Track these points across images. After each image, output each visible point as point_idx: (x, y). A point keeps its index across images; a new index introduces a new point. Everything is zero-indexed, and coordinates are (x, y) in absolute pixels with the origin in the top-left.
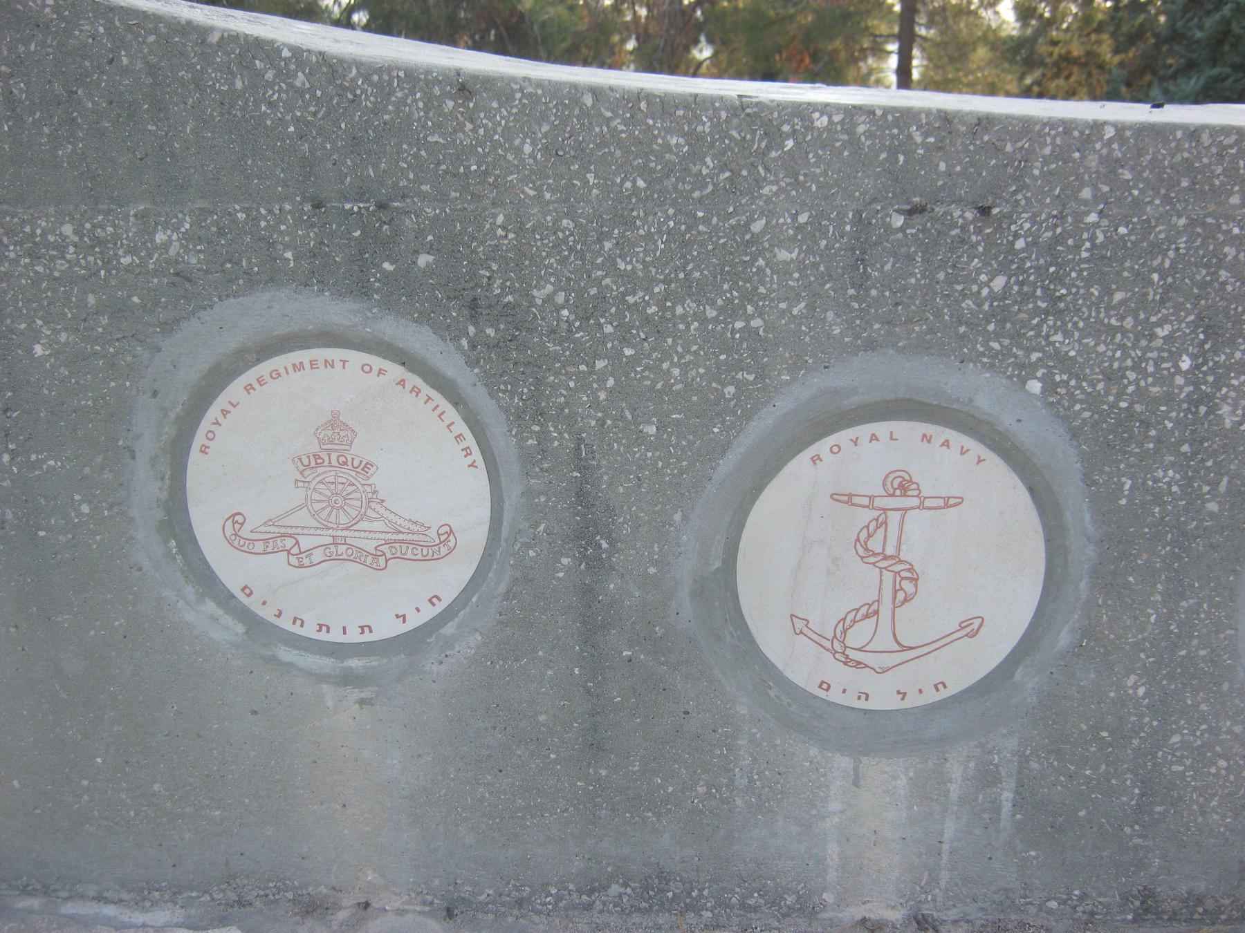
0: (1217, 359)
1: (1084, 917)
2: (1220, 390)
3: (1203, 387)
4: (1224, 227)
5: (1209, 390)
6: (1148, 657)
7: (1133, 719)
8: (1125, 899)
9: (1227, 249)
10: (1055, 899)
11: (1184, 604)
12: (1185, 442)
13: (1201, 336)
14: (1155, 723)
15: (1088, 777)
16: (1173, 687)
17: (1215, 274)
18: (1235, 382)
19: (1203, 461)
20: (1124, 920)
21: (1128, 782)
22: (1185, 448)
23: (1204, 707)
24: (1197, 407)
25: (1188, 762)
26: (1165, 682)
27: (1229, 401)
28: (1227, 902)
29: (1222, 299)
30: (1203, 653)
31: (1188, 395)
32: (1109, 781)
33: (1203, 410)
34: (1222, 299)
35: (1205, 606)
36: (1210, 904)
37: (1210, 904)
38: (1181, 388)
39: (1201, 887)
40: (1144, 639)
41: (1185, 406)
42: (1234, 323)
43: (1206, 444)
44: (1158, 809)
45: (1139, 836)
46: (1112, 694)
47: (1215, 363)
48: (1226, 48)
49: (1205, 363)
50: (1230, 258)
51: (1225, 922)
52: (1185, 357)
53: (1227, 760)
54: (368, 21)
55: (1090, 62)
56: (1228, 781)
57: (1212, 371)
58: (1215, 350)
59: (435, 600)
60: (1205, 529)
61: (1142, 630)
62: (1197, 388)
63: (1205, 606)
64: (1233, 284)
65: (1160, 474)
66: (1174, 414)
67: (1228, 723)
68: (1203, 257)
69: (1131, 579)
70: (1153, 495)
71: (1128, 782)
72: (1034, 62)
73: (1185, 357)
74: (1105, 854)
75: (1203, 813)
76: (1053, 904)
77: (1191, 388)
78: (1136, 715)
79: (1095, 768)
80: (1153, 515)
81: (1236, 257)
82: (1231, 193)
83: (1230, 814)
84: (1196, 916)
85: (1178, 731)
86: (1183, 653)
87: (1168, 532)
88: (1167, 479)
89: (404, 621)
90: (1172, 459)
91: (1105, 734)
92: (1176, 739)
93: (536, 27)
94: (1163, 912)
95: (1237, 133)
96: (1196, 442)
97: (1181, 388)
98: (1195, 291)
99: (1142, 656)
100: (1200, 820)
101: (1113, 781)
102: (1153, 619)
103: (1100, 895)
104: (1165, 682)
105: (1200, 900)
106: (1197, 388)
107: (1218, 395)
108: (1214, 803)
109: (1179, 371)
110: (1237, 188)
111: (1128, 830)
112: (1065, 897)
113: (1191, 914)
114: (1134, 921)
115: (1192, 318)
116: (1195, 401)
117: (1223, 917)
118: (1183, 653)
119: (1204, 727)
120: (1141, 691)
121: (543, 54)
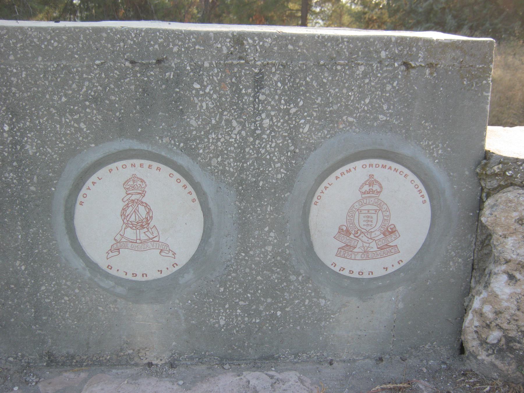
0: (19, 125)
1: (25, 365)
2: (24, 139)
3: (16, 138)
4: (9, 69)
5: (19, 139)
6: (22, 253)
7: (23, 279)
8: (41, 357)
9: (12, 79)
10: (11, 357)
11: (31, 230)
12: (14, 161)
13: (10, 116)
14: (33, 281)
15: (10, 305)
16: (36, 266)
17: (10, 89)
18: (29, 135)
19: (24, 169)
20: (43, 365)
21: (28, 307)
22: (15, 164)
23: (51, 274)
24: (16, 146)
25: (52, 298)
26: (32, 264)
27: (29, 143)
28: (85, 357)
29: (15, 100)
30: (45, 251)
31: (11, 141)
32: (20, 306)
33: (18, 147)
34: (15, 100)
35: (41, 231)
36: (77, 358)
37: (77, 358)
38: (7, 138)
39: (72, 351)
40: (18, 245)
41: (10, 146)
42: (23, 110)
43: (23, 162)
44: (44, 318)
45: (40, 330)
46: (11, 269)
47: (19, 127)
48: (432, 15)
49: (15, 127)
50: (14, 82)
51: (86, 366)
52: (5, 125)
53: (68, 297)
54: (307, 16)
55: (384, 23)
56: (71, 305)
57: (19, 130)
58: (18, 122)
59: (175, 265)
60: (32, 198)
61: (16, 242)
62: (14, 138)
63: (41, 231)
64: (19, 94)
65: (7, 175)
66: (6, 149)
67: (64, 281)
68: (3, 82)
69: (6, 220)
70: (6, 184)
71: (28, 307)
72: (363, 21)
73: (5, 125)
74: (27, 337)
75: (64, 320)
76: (11, 359)
77: (11, 138)
78: (24, 278)
79: (13, 301)
80: (8, 192)
81: (17, 82)
82: (9, 55)
83: (75, 320)
84: (73, 364)
85: (43, 284)
86: (36, 251)
87: (16, 200)
88: (11, 177)
89: (161, 273)
90: (11, 168)
91: (12, 286)
92: (43, 288)
93: (152, 7)
94: (59, 362)
95: (6, 29)
96: (20, 161)
97: (7, 138)
98: (3, 96)
99: (19, 252)
100: (63, 322)
101: (22, 306)
102: (20, 236)
103: (30, 355)
104: (32, 264)
105: (73, 357)
106: (14, 138)
107: (24, 141)
108: (67, 315)
109: (4, 131)
110: (11, 53)
111: (34, 327)
112: (15, 356)
113: (71, 363)
114: (48, 365)
115: (4, 108)
116: (15, 144)
117: (85, 364)
118: (36, 251)
119: (54, 283)
120: (23, 268)
121: (155, 17)
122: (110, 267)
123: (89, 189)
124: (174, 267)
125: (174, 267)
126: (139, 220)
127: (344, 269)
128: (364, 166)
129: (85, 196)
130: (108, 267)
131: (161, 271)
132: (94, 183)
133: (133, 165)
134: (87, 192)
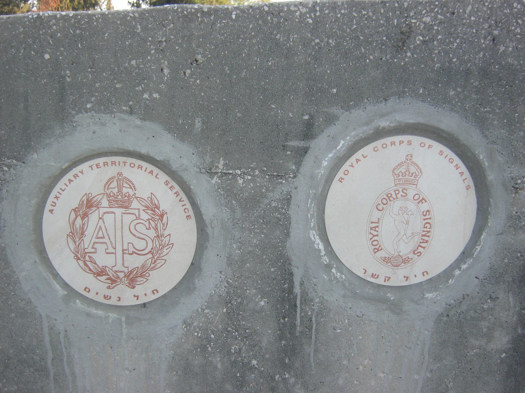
89: (137, 299)
122: (87, 290)
123: (352, 166)
124: (154, 294)
125: (154, 294)
126: (118, 235)
127: (389, 278)
128: (423, 145)
129: (346, 172)
130: (85, 290)
131: (138, 297)
132: (358, 160)
133: (409, 143)
134: (350, 169)
